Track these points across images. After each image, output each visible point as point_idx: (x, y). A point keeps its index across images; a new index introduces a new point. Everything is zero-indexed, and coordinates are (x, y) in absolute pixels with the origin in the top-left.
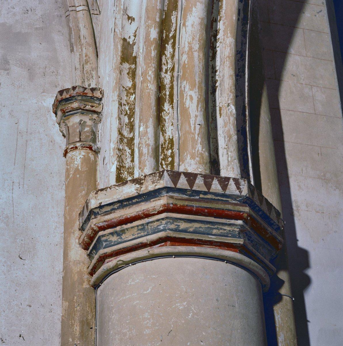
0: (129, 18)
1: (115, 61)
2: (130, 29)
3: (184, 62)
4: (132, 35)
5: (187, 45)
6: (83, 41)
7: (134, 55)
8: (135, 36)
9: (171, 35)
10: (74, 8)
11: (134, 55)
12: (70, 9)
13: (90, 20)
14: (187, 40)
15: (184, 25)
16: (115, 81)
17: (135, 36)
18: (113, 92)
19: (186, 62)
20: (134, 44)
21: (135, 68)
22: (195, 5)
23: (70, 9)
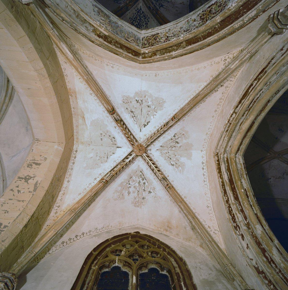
0: (251, 259)
1: (255, 274)
2: (254, 262)
3: (283, 266)
4: (255, 264)
5: (279, 260)
6: (237, 276)
7: (261, 271)
8: (257, 264)
9: (270, 260)
10: (227, 265)
11: (261, 271)
12: (226, 266)
13: (239, 144)
14: (278, 259)
15: (273, 255)
16: (261, 282)
17: (257, 264)
18: (263, 286)
19: (284, 266)
20: (258, 267)
21: (265, 275)
22: (273, 247)
23: (226, 266)
